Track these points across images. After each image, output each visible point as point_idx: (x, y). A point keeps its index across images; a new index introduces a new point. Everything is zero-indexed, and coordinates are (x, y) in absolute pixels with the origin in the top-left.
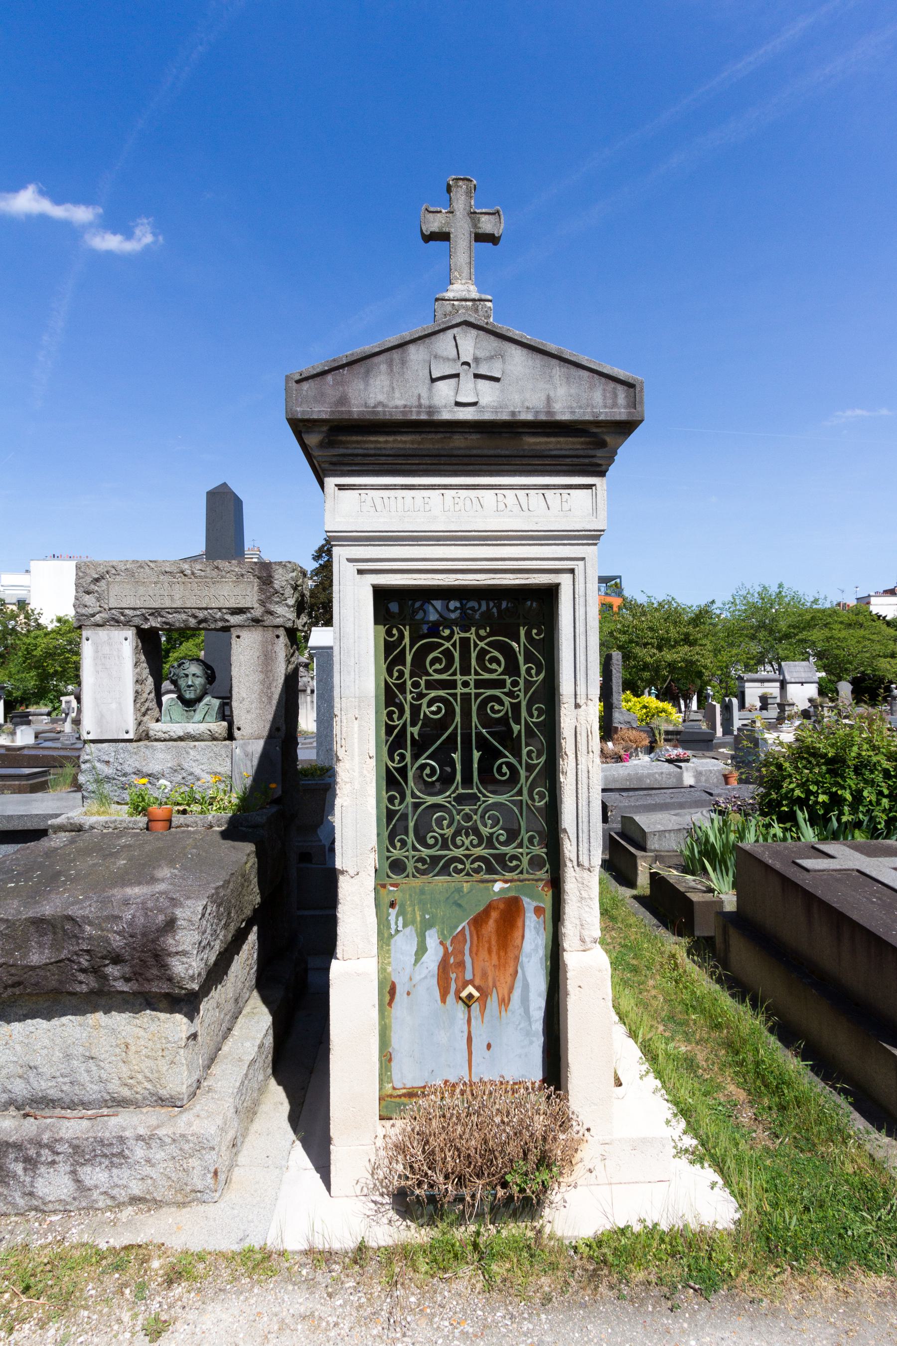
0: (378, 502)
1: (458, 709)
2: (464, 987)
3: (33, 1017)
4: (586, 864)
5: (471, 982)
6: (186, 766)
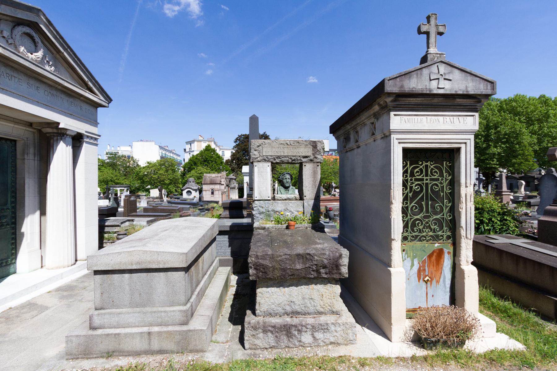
0: (419, 120)
1: (424, 188)
2: (425, 277)
3: (292, 286)
4: (469, 238)
5: (427, 275)
6: (289, 208)
